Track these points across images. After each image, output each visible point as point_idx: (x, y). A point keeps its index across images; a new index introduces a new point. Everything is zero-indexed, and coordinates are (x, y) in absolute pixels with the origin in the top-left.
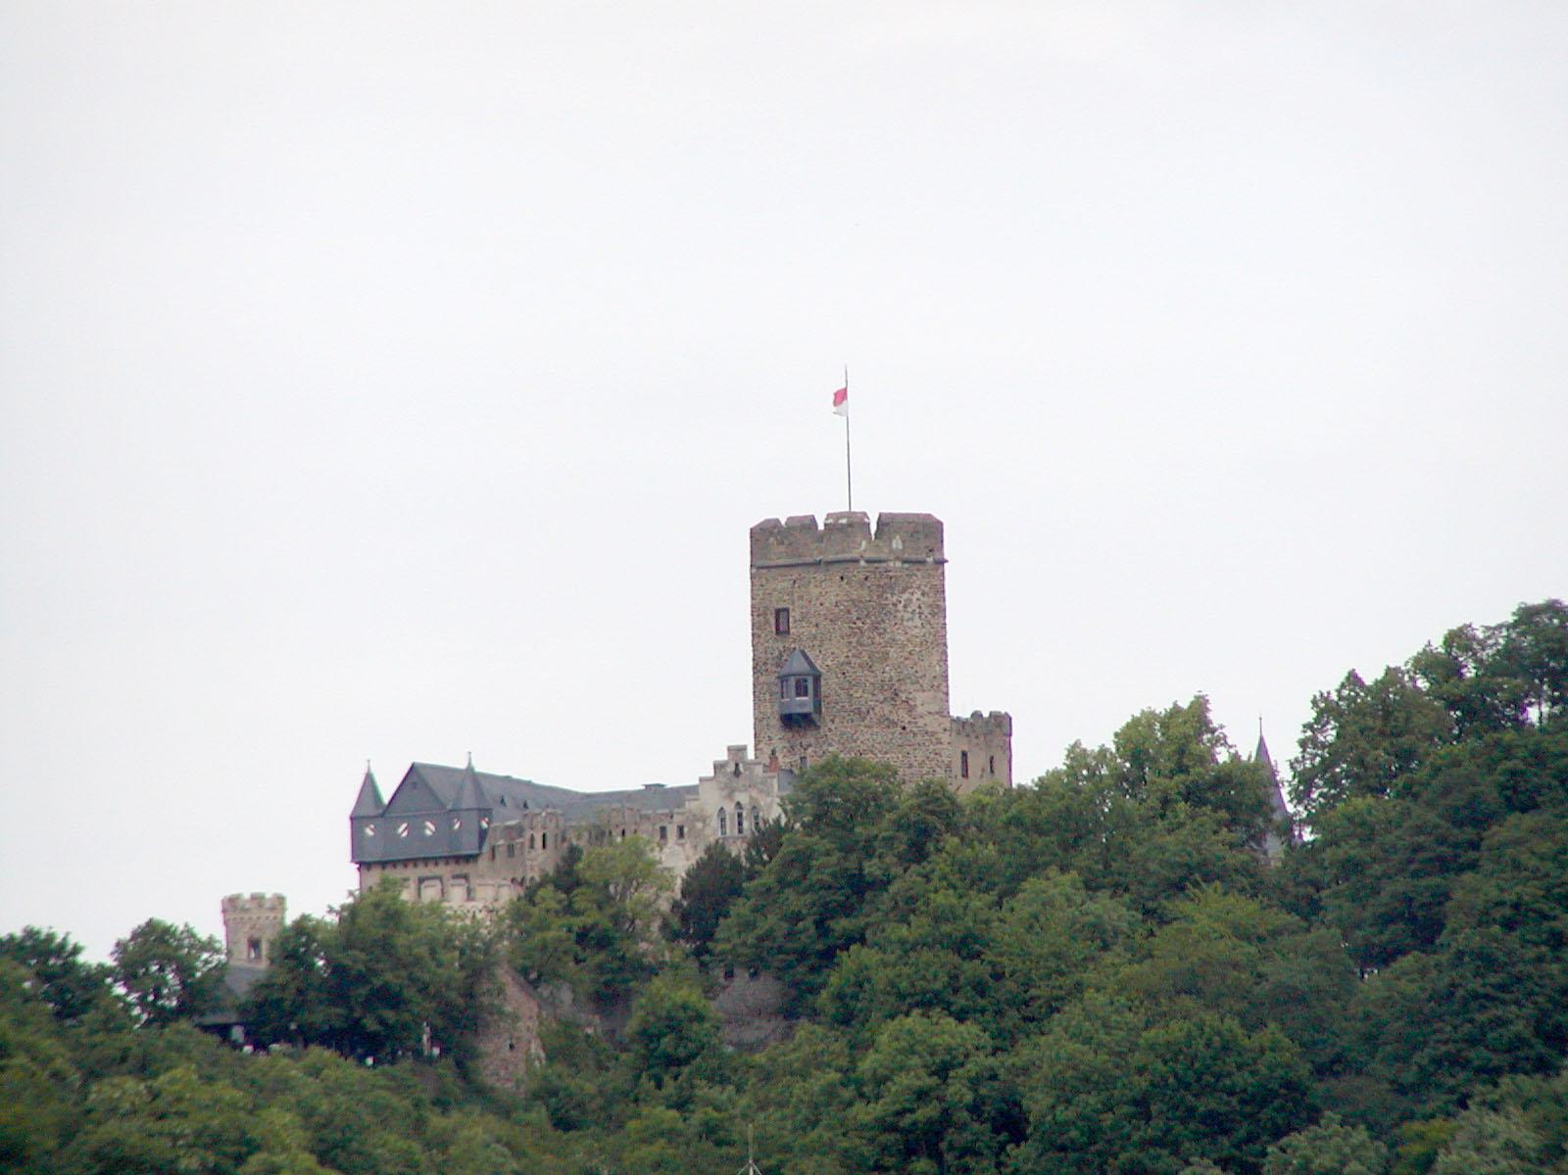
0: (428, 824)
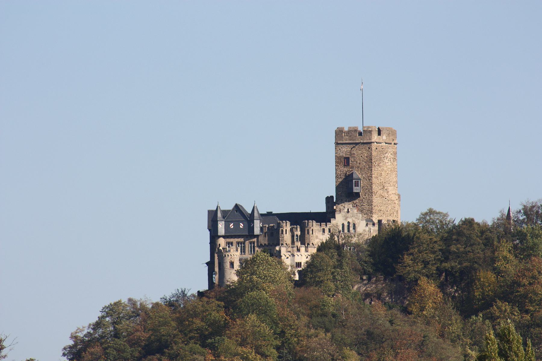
0: (241, 224)
